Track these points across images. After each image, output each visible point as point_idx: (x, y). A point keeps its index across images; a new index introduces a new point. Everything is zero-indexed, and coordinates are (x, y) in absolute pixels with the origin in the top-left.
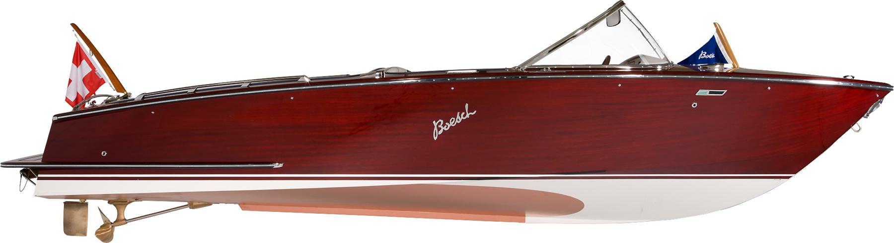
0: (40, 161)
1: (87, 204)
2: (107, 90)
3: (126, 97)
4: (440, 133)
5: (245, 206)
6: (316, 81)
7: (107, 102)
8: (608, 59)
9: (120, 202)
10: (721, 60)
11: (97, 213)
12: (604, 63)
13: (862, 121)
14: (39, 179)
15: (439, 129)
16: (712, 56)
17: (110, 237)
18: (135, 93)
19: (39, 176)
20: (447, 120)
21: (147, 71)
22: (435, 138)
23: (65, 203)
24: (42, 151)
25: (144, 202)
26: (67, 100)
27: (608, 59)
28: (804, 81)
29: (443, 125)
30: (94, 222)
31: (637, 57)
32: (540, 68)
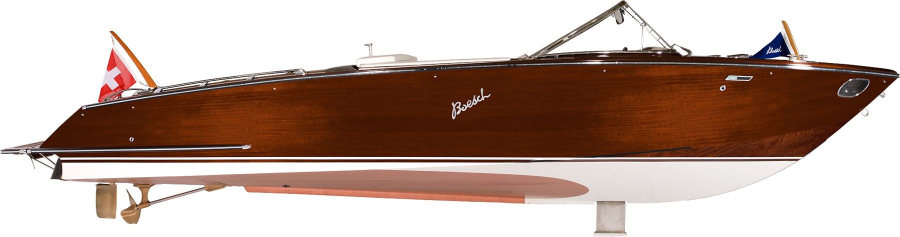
0: (38, 147)
2: (141, 84)
4: (458, 113)
6: (308, 74)
8: (57, 174)
9: (144, 184)
10: (785, 52)
11: (125, 195)
15: (457, 110)
20: (464, 102)
21: (175, 64)
30: (123, 203)
32: (553, 56)
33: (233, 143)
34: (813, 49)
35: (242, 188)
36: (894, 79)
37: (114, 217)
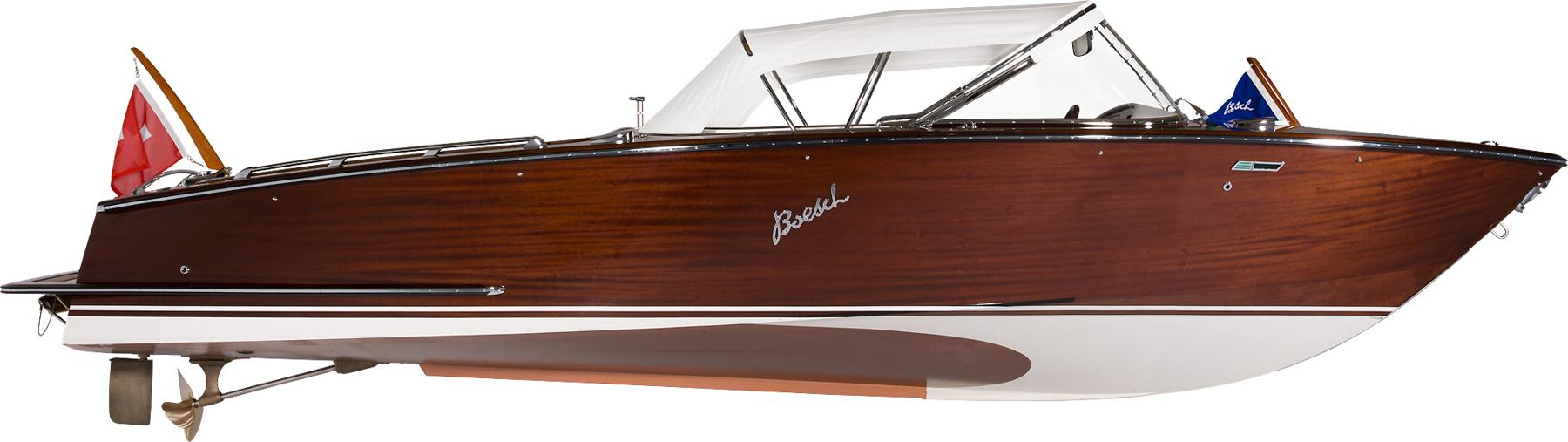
0: (74, 282)
2: (192, 162)
4: (785, 232)
5: (433, 366)
7: (188, 182)
8: (1075, 111)
9: (212, 359)
10: (1262, 110)
11: (171, 377)
12: (1069, 115)
13: (1512, 219)
14: (72, 313)
15: (783, 226)
18: (237, 163)
19: (73, 308)
20: (798, 211)
21: (258, 126)
22: (776, 242)
23: (113, 361)
24: (77, 268)
25: (392, 365)
27: (1075, 111)
28: (644, 150)
29: (792, 220)
31: (1132, 106)
32: (957, 124)
33: (390, 279)
34: (1332, 99)
37: (145, 420)
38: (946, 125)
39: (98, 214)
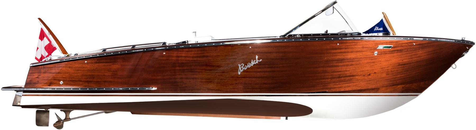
1: (49, 111)
3: (68, 56)
4: (242, 71)
8: (287, 119)
9: (67, 108)
10: (386, 33)
11: (54, 115)
15: (242, 69)
16: (381, 29)
17: (61, 127)
21: (82, 42)
22: (239, 73)
23: (37, 111)
26: (36, 58)
32: (295, 35)
35: (130, 113)
36: (472, 46)
38: (291, 35)
39: (31, 67)
